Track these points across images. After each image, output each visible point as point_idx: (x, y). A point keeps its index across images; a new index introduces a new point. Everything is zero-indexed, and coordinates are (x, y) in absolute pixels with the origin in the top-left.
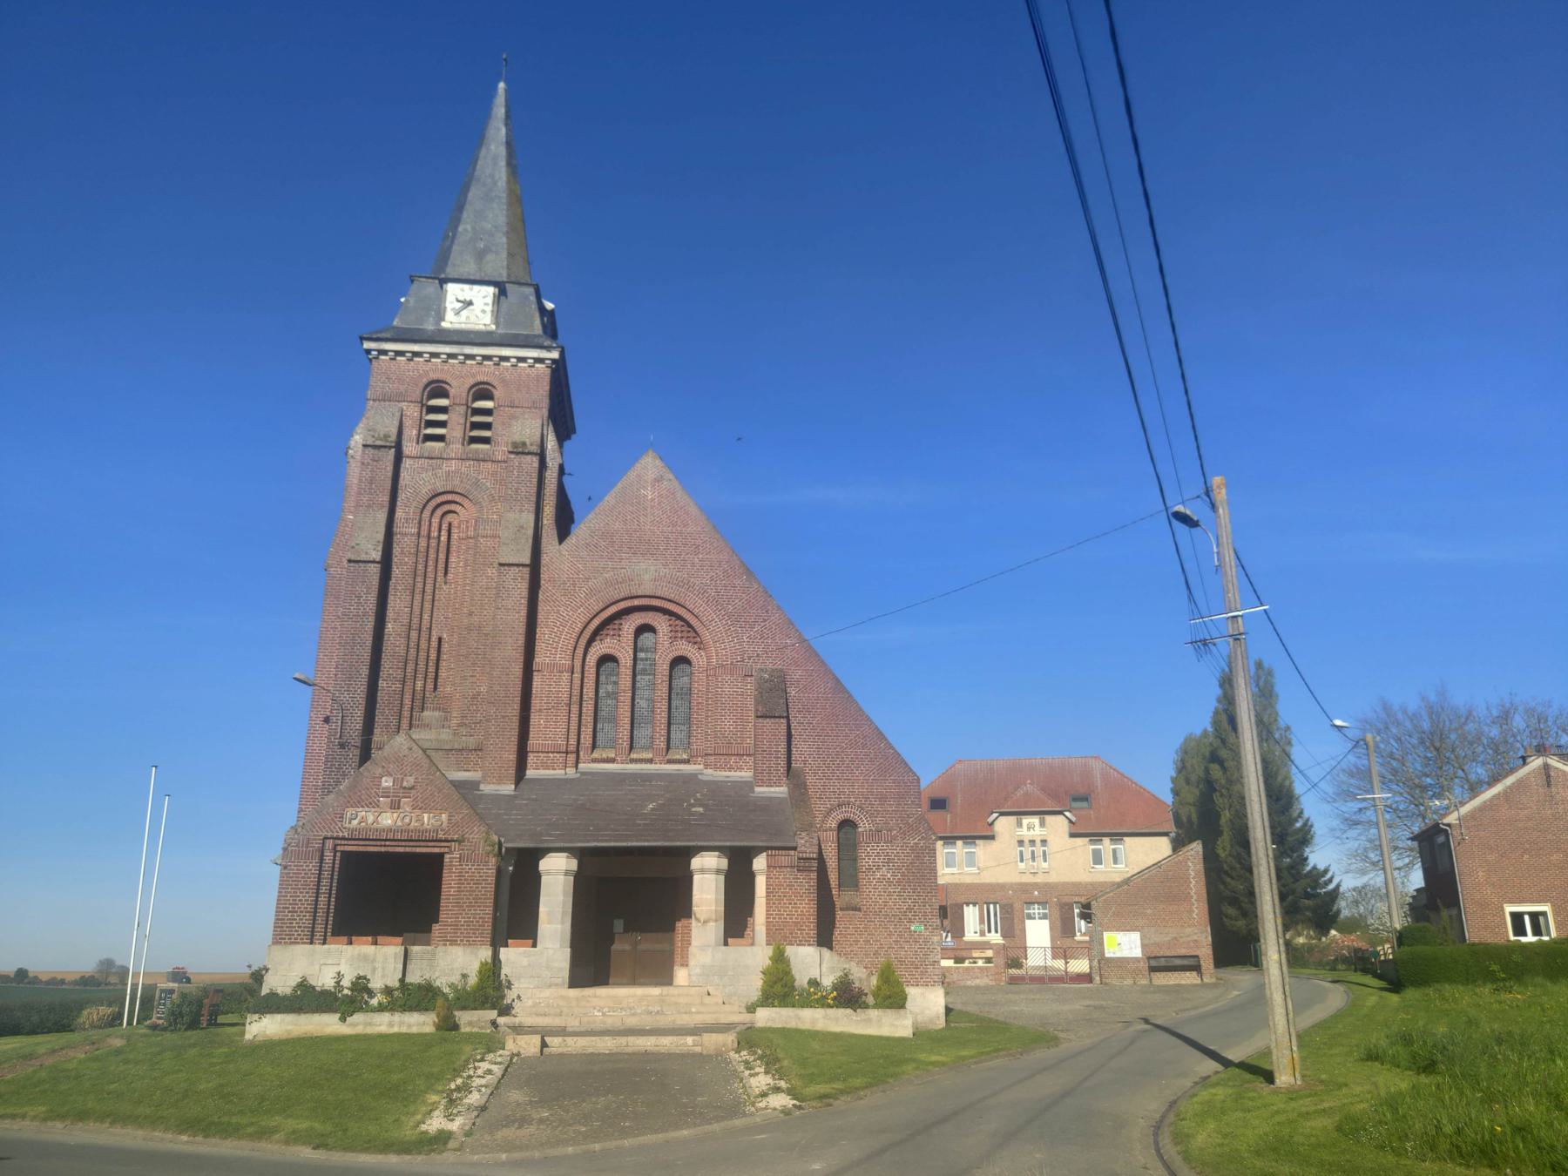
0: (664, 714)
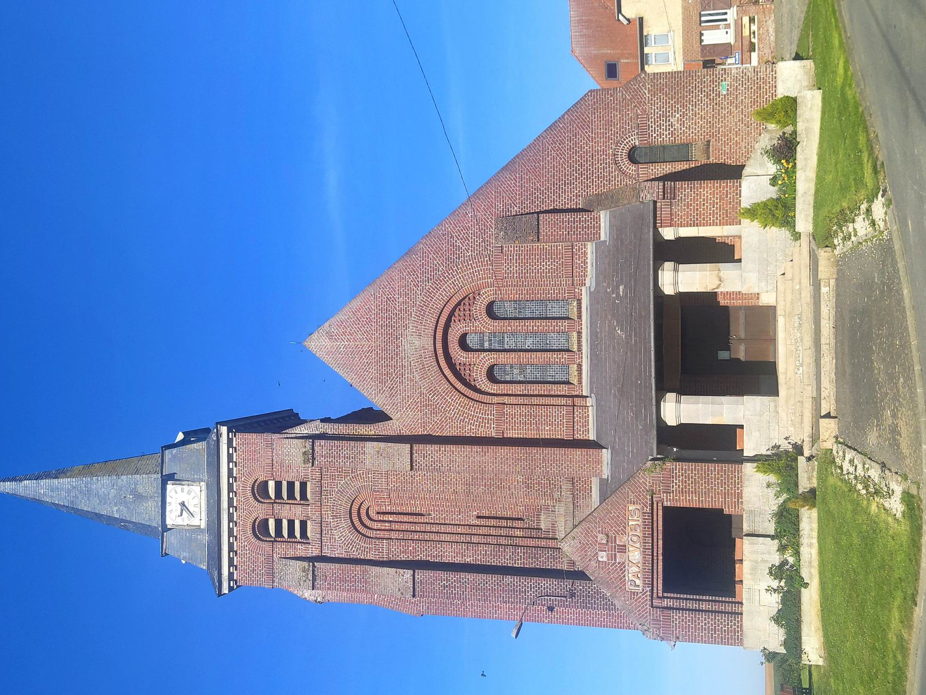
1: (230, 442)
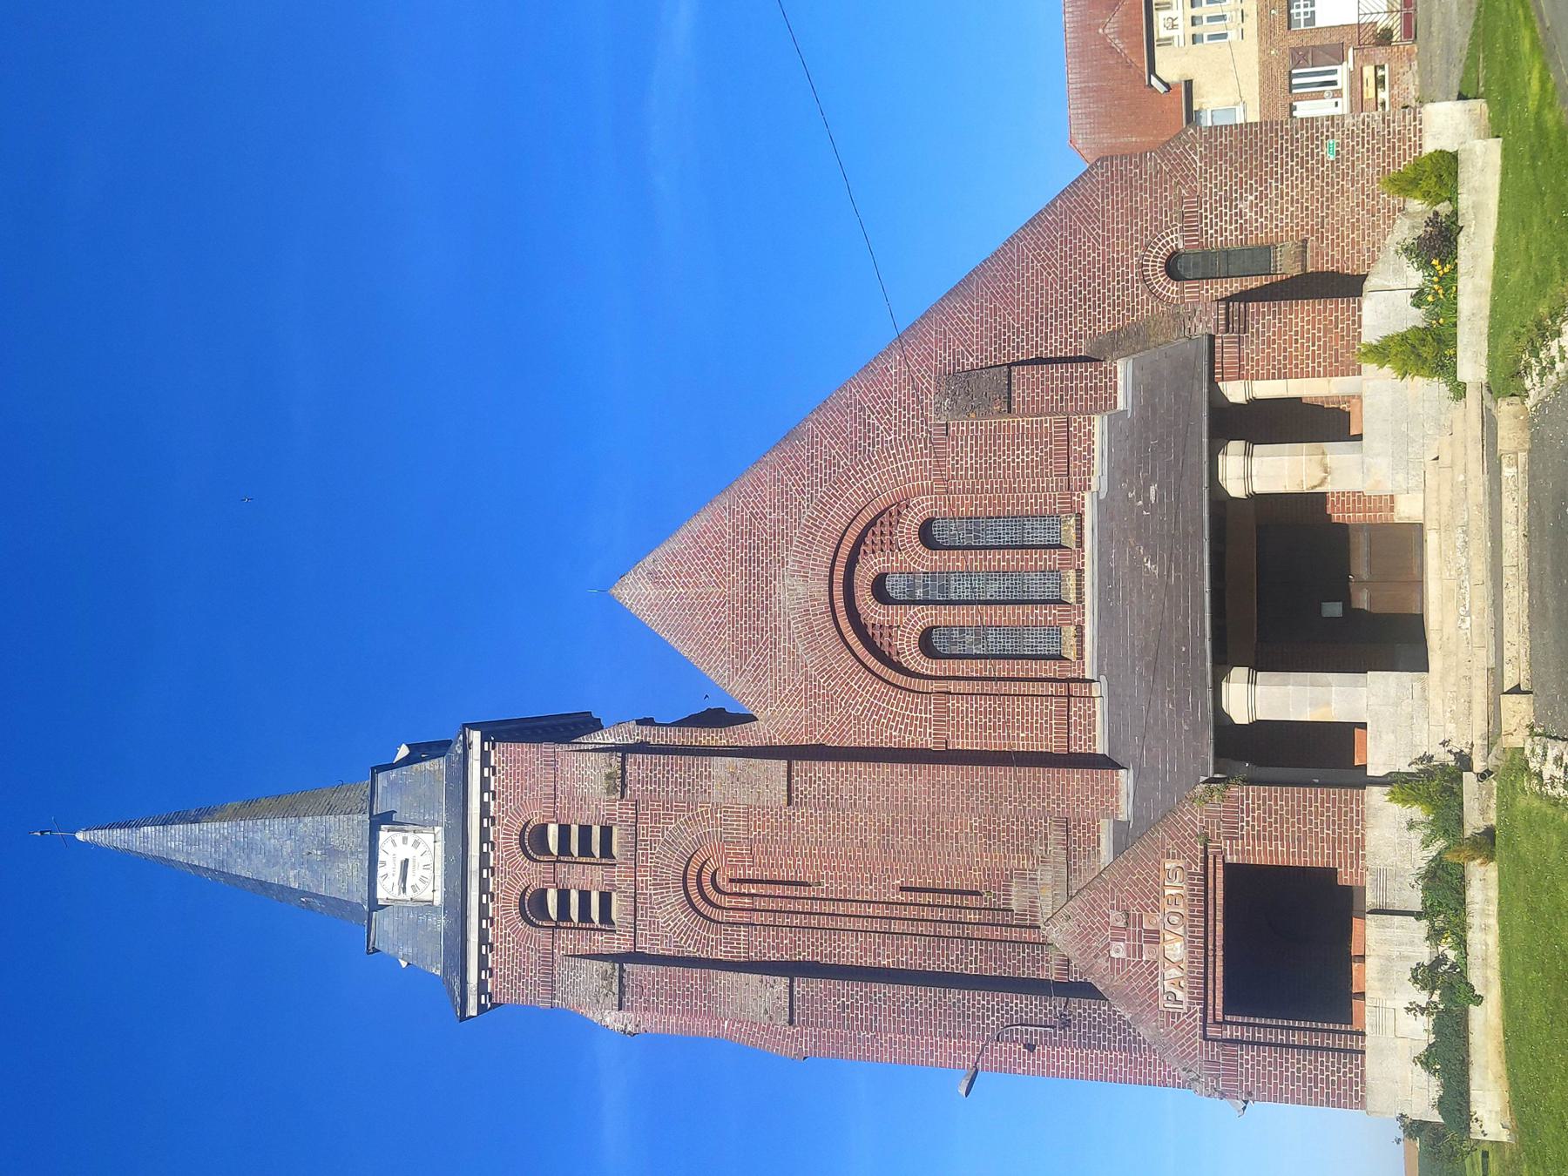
0: (1008, 554)
1: (485, 758)
